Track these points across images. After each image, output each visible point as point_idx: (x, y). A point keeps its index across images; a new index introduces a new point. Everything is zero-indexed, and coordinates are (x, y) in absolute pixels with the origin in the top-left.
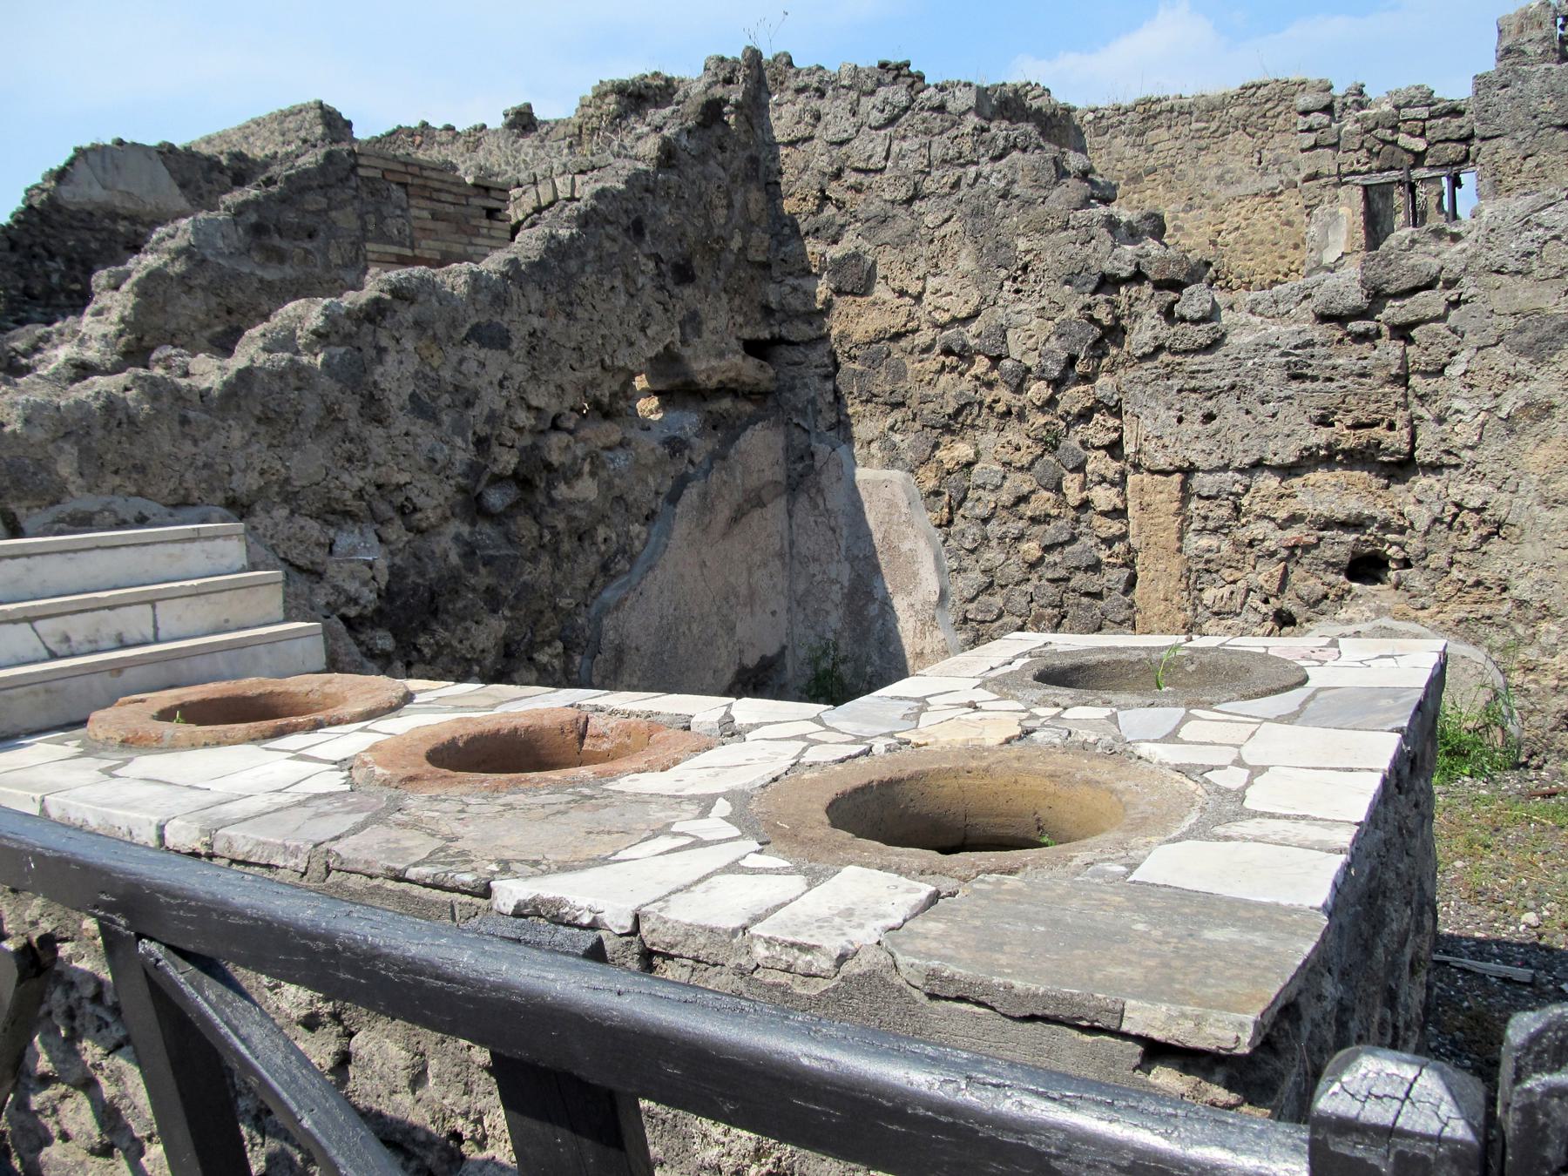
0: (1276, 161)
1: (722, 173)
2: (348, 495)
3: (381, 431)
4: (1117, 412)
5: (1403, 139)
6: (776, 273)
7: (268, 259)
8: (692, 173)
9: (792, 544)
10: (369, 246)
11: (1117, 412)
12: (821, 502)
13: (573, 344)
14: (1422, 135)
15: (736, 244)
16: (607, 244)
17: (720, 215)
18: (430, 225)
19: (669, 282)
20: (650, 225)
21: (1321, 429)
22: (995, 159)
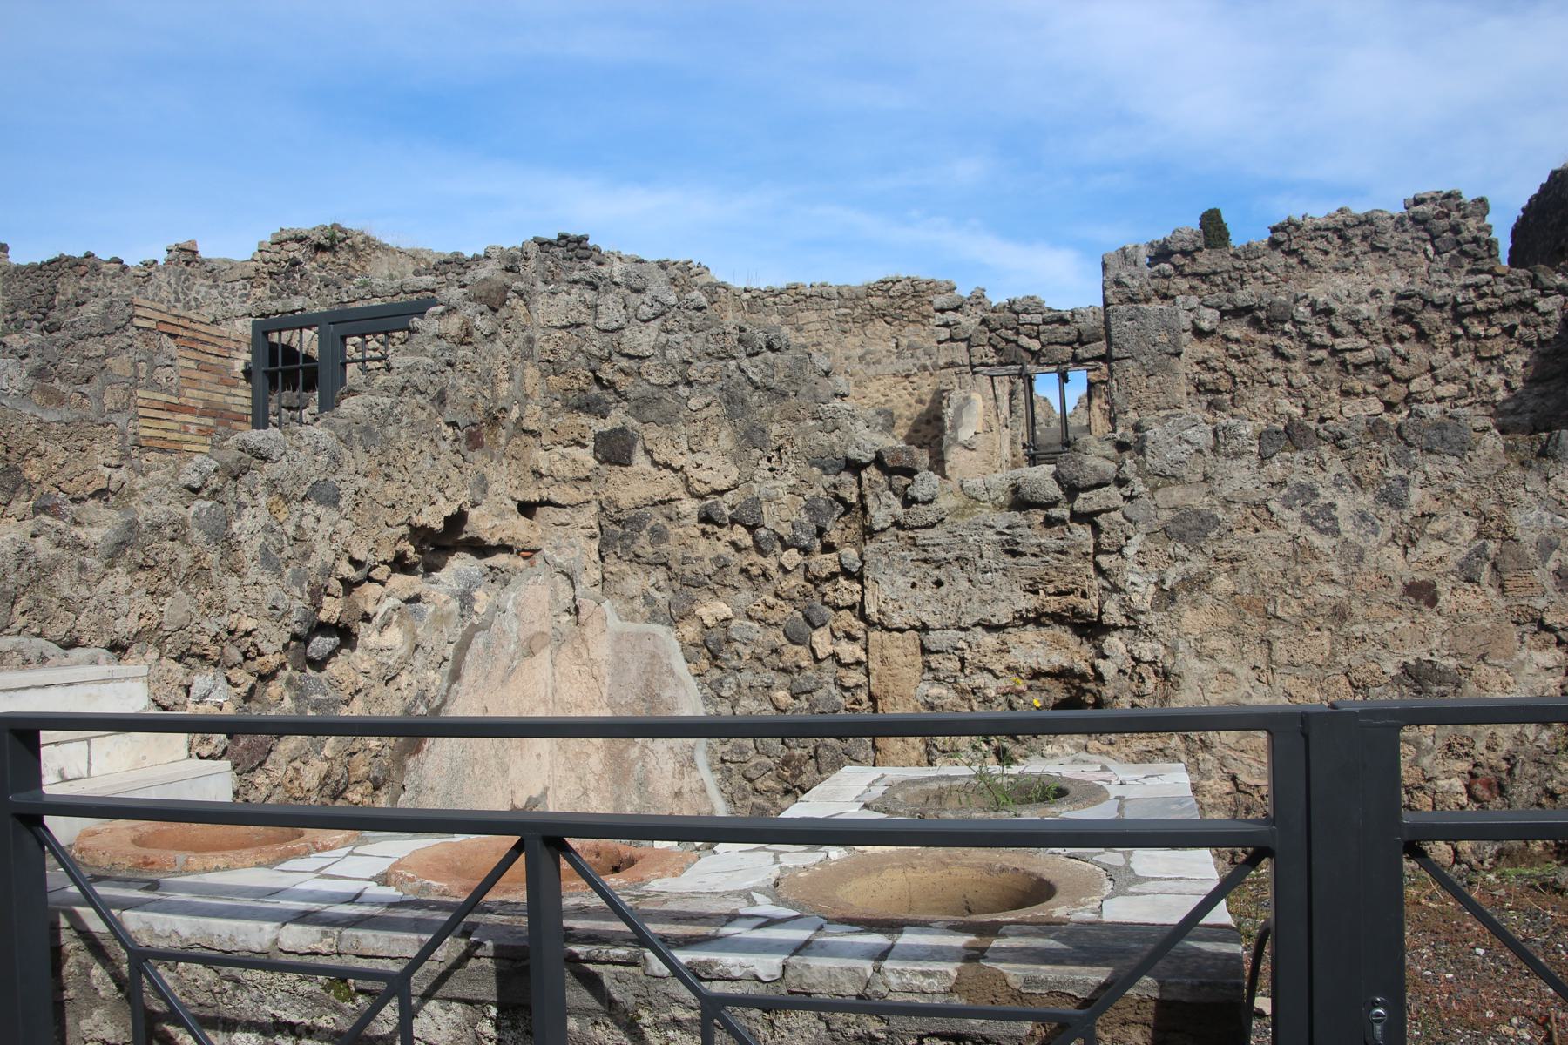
0: (910, 347)
1: (506, 351)
2: (206, 640)
3: (235, 580)
4: (860, 578)
5: (1024, 341)
6: (546, 440)
7: (49, 401)
8: (484, 349)
9: (555, 690)
10: (140, 393)
11: (860, 578)
12: (584, 652)
13: (389, 503)
14: (1037, 337)
15: (514, 414)
16: (418, 412)
17: (504, 389)
18: (196, 375)
19: (462, 447)
20: (450, 394)
21: (1029, 595)
22: (749, 356)
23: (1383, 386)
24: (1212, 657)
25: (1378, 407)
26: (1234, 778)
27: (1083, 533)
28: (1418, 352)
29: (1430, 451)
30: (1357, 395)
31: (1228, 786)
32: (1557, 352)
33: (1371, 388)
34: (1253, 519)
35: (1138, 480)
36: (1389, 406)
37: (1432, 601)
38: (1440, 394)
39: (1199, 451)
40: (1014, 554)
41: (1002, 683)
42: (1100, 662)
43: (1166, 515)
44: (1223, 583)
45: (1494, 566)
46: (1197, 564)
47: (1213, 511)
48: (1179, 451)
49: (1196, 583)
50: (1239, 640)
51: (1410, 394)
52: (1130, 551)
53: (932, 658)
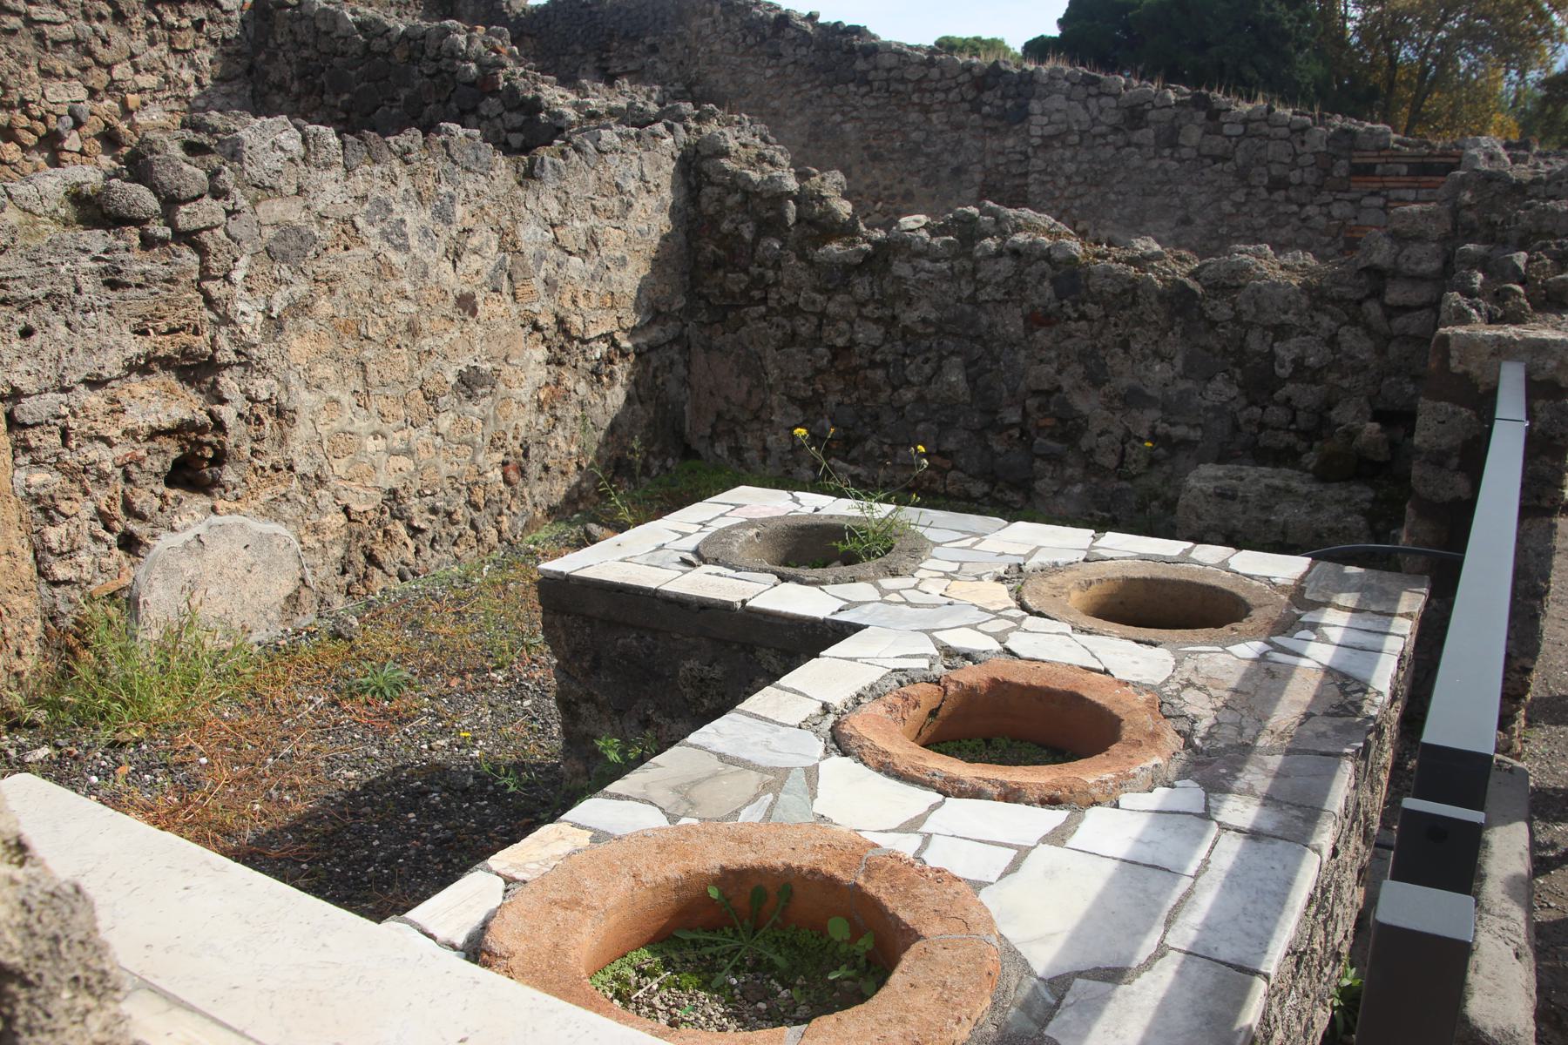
21: (139, 338)
23: (84, 69)
24: (319, 387)
25: (82, 94)
26: (346, 510)
27: (189, 258)
28: (118, 36)
29: (468, 170)
30: (58, 77)
31: (342, 518)
32: (238, 53)
33: (74, 72)
34: (344, 237)
35: (237, 191)
36: (93, 93)
37: (474, 312)
38: (141, 85)
39: (292, 160)
40: (113, 285)
41: (119, 451)
42: (217, 408)
43: (269, 232)
44: (324, 306)
45: (510, 276)
46: (301, 288)
47: (310, 228)
48: (274, 161)
49: (301, 308)
50: (339, 365)
51: (113, 81)
52: (237, 276)
53: (30, 434)
